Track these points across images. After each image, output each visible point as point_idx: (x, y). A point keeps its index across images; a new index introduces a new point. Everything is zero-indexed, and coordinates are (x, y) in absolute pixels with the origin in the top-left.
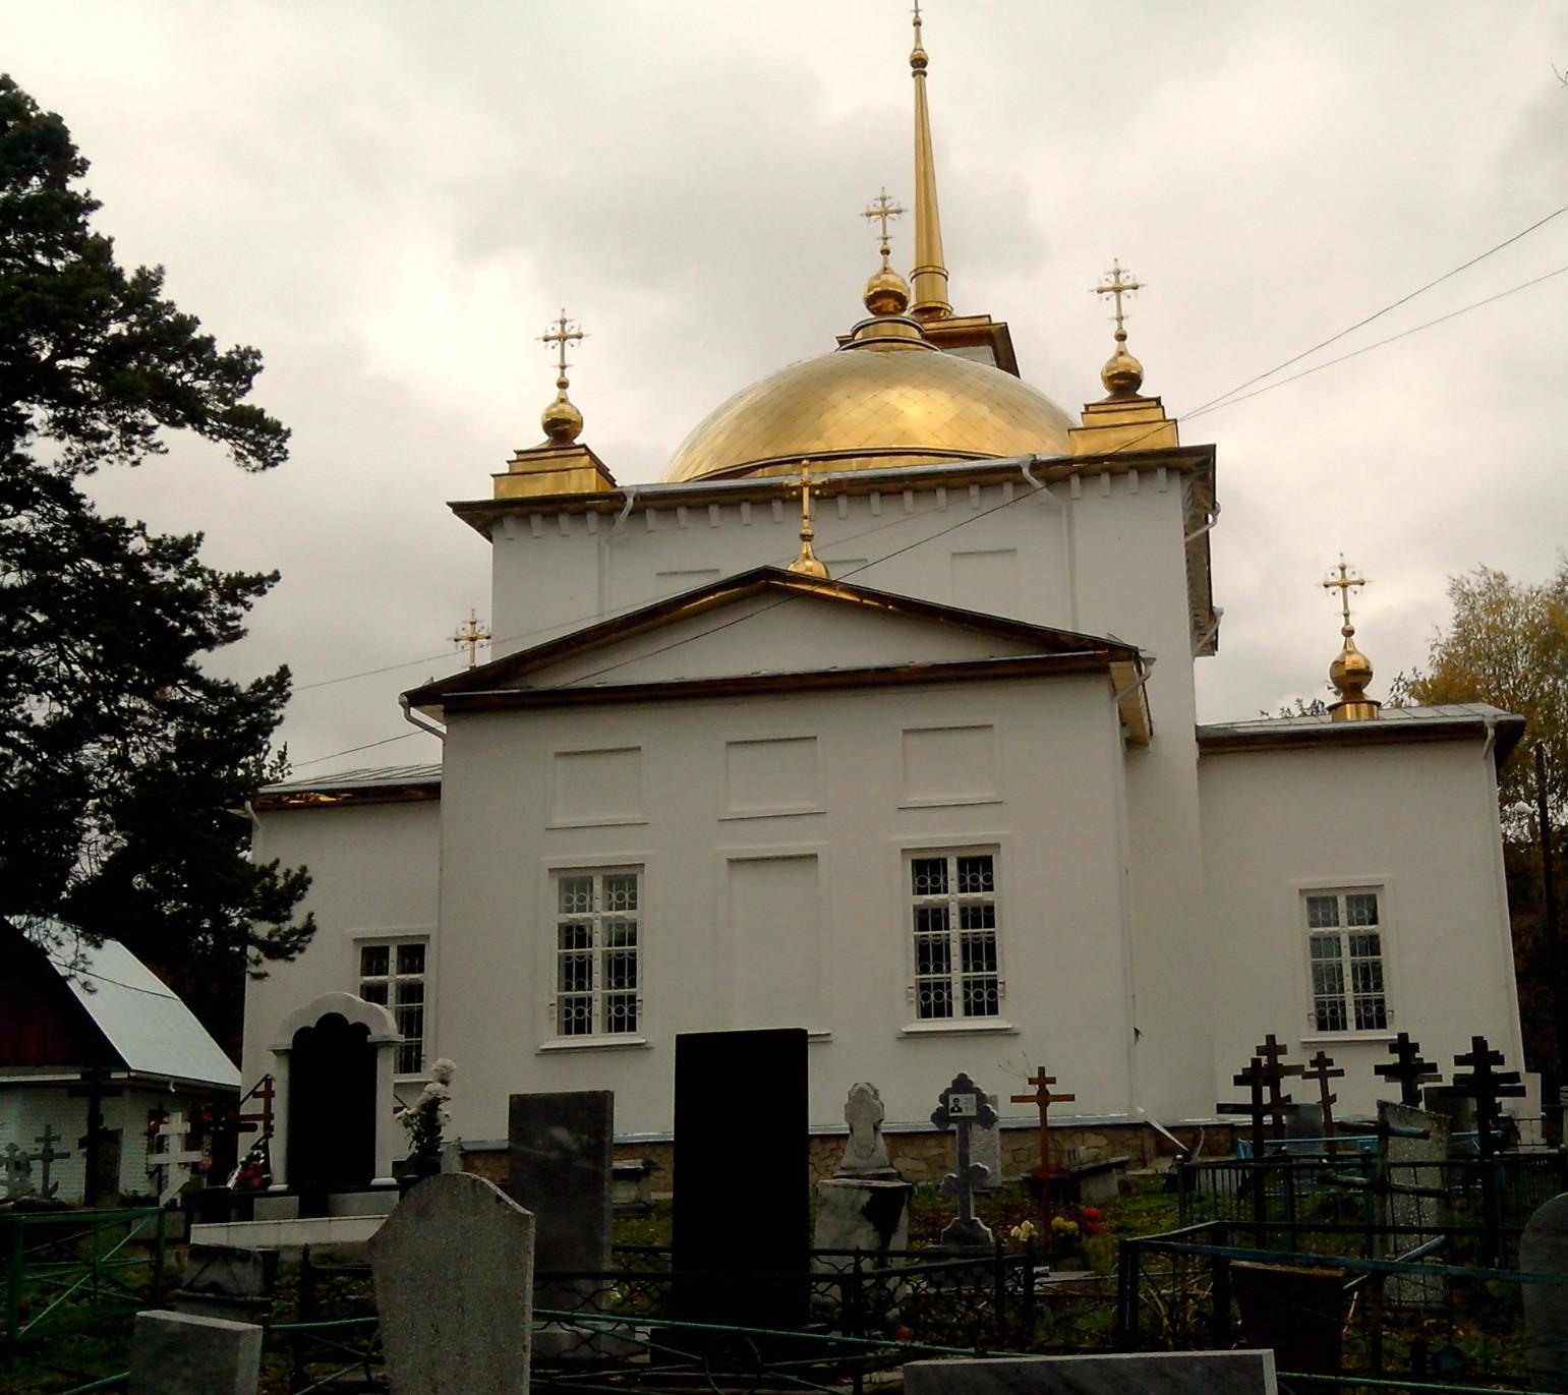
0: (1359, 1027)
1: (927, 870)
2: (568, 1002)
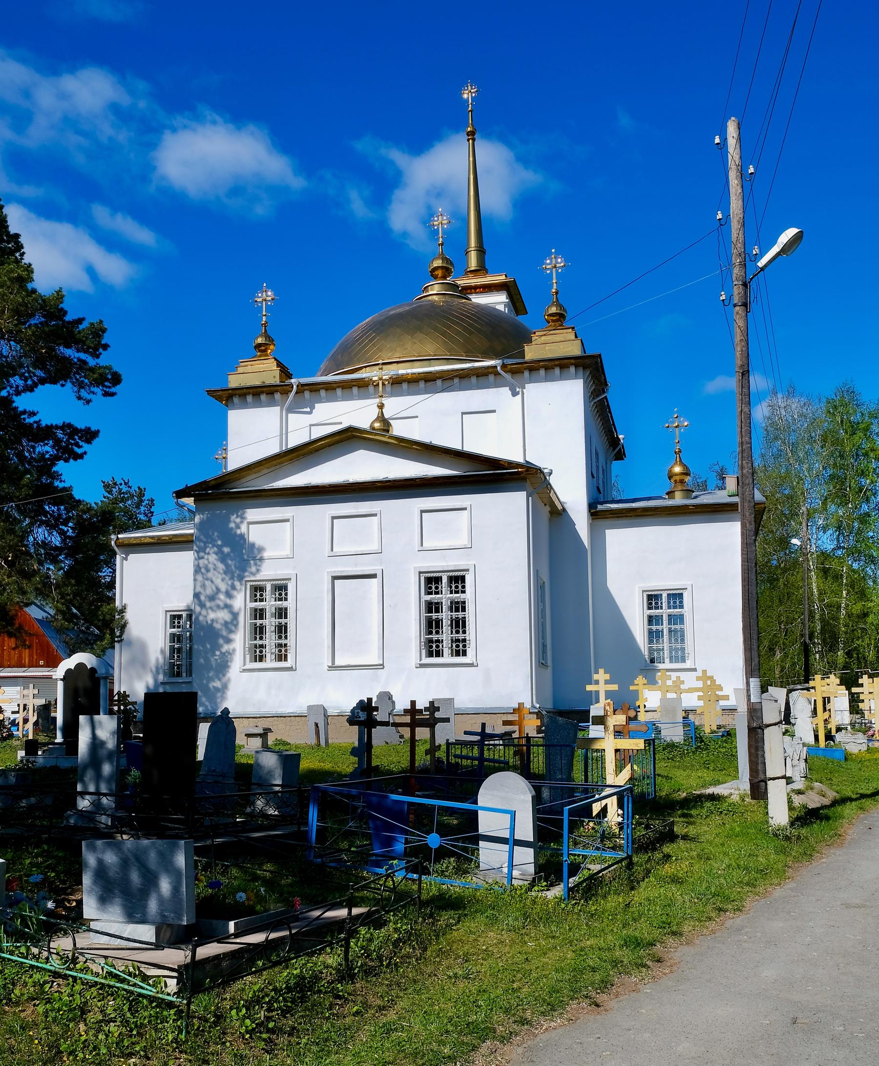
0: (671, 662)
1: (432, 582)
2: (256, 646)
